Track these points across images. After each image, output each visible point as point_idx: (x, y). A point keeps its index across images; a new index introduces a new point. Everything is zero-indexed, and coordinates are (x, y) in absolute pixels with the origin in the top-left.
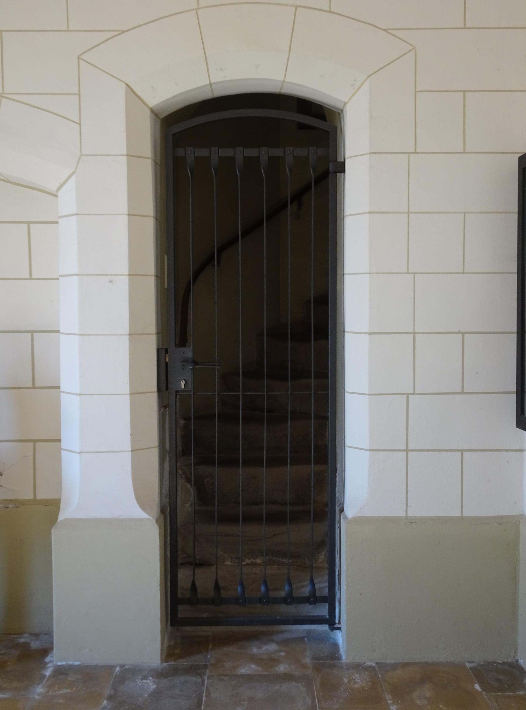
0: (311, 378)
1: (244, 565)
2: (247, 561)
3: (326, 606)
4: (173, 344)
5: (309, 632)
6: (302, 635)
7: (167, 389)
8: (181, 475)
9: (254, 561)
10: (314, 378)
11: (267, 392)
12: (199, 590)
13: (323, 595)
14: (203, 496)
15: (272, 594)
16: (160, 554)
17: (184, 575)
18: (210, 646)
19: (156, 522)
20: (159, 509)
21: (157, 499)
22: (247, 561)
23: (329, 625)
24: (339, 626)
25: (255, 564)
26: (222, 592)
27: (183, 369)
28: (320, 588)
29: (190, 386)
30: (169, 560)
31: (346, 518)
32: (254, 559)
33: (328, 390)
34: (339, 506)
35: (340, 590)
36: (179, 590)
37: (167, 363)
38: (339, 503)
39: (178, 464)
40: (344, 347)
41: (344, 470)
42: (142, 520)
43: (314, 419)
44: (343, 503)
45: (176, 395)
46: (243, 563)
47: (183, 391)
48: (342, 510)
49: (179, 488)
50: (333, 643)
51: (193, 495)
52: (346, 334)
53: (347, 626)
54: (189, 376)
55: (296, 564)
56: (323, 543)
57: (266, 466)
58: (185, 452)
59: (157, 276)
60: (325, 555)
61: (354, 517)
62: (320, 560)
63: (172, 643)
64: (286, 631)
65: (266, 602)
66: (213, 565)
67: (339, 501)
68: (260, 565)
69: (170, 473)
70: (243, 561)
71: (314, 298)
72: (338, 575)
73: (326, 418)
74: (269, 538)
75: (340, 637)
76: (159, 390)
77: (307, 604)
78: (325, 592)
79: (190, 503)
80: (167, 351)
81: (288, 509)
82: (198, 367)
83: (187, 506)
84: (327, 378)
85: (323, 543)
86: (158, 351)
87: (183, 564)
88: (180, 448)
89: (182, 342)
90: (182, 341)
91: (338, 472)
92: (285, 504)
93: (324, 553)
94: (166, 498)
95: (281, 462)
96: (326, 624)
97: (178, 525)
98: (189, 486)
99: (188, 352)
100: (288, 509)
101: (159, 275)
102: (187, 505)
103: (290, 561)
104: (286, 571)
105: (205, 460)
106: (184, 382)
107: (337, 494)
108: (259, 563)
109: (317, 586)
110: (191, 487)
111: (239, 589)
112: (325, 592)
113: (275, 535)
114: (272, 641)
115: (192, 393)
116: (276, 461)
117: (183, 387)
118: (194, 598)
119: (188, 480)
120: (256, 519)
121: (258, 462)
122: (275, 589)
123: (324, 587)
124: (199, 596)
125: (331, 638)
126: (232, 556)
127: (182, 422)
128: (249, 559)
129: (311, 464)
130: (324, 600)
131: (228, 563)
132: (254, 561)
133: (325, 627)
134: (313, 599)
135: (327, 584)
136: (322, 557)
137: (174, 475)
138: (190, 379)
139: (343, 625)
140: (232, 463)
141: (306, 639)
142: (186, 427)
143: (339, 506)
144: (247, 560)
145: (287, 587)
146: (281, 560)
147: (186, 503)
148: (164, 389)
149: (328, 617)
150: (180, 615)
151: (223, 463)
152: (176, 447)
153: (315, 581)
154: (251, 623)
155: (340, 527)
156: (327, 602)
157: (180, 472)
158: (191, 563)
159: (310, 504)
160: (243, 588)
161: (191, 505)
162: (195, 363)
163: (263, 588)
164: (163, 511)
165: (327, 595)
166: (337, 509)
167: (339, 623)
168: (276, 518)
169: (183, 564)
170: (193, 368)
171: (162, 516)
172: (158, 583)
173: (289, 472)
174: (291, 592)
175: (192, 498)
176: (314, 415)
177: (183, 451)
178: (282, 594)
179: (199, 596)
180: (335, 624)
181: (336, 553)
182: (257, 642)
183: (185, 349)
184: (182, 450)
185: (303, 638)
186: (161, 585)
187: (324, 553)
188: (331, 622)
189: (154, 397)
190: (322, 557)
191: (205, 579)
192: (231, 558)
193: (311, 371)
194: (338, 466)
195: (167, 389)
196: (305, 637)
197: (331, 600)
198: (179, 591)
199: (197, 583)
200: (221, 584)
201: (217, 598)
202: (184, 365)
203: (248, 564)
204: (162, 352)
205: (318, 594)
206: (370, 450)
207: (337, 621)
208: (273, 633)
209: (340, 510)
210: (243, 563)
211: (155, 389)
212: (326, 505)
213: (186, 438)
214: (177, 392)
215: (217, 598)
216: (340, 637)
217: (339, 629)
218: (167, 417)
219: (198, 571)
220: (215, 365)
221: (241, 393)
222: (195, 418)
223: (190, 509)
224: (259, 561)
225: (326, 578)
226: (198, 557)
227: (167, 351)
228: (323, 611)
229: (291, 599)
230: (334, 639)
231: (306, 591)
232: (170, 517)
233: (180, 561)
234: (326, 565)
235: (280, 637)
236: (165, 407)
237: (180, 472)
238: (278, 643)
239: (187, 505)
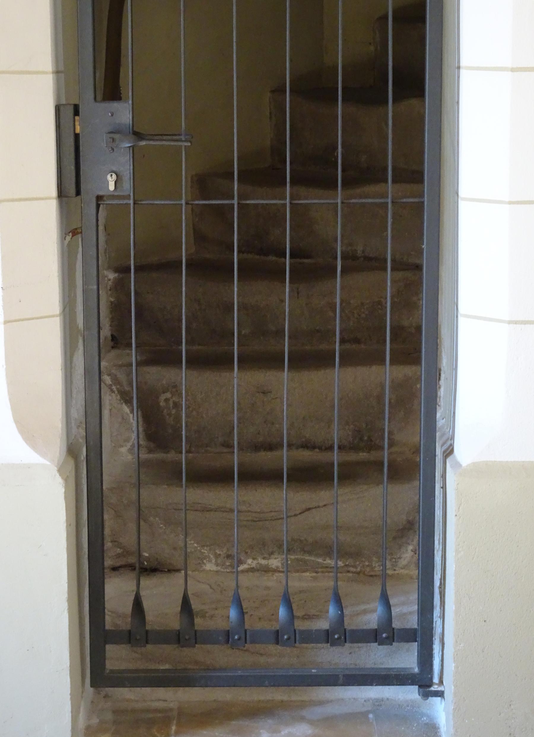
0: (386, 181)
1: (242, 571)
2: (250, 563)
3: (414, 646)
4: (90, 95)
5: (378, 703)
6: (364, 709)
7: (78, 193)
8: (110, 387)
9: (263, 562)
10: (394, 181)
11: (292, 198)
12: (150, 617)
13: (408, 626)
14: (157, 431)
15: (300, 625)
16: (60, 296)
17: (118, 591)
18: (174, 728)
19: (59, 471)
20: (65, 449)
21: (60, 425)
22: (250, 563)
23: (420, 687)
24: (440, 689)
25: (267, 570)
26: (198, 621)
27: (113, 149)
28: (403, 615)
29: (127, 186)
30: (86, 556)
31: (458, 465)
32: (264, 558)
33: (423, 197)
34: (442, 446)
35: (443, 617)
36: (107, 618)
37: (77, 137)
38: (444, 438)
39: (103, 364)
40: (458, 103)
41: (455, 368)
42: (29, 466)
43: (392, 269)
44: (453, 438)
45: (98, 206)
46: (241, 568)
47: (112, 197)
48: (449, 452)
49: (106, 413)
50: (426, 724)
51: (135, 428)
52: (463, 72)
53: (456, 686)
54: (124, 162)
55: (352, 569)
56: (408, 527)
57: (289, 367)
58: (118, 341)
59: (57, 72)
60: (414, 551)
61: (474, 464)
62: (403, 562)
63: (95, 721)
64: (328, 702)
65: (289, 639)
66: (178, 570)
67: (443, 435)
68: (276, 571)
69: (87, 372)
70: (240, 562)
71: (394, 12)
72: (440, 588)
73: (418, 268)
74: (295, 515)
75: (441, 711)
76: (61, 194)
77: (376, 644)
78: (413, 622)
79: (129, 445)
80: (76, 112)
81: (336, 457)
82: (143, 143)
83: (123, 449)
84: (422, 181)
85: (408, 527)
86: (58, 109)
87: (114, 569)
88: (106, 332)
89: (112, 92)
90: (111, 90)
91: (443, 376)
92: (330, 448)
93: (410, 547)
94: (78, 427)
95: (323, 360)
96: (412, 684)
97: (104, 488)
98: (126, 409)
99: (123, 113)
100: (336, 457)
101: (62, 68)
102: (124, 450)
103: (340, 564)
104: (332, 583)
105: (161, 356)
106: (114, 176)
107: (440, 423)
108: (273, 566)
109: (395, 611)
110: (132, 411)
111: (233, 613)
112: (413, 622)
113: (309, 509)
114: (302, 719)
115: (131, 202)
116: (310, 358)
117: (112, 187)
118: (138, 631)
119: (126, 398)
120: (270, 477)
121: (273, 361)
122: (307, 617)
123: (411, 613)
124: (148, 627)
125: (423, 715)
126: (218, 552)
127: (112, 276)
128: (254, 559)
129: (385, 364)
130: (409, 636)
131: (210, 566)
132: (263, 562)
133: (410, 693)
134: (386, 634)
135: (416, 607)
136: (408, 554)
137: (94, 377)
138: (127, 170)
139: (448, 687)
140: (221, 362)
141: (371, 716)
142: (120, 286)
143: (442, 446)
144: (250, 561)
145: (332, 610)
146: (320, 560)
147: (122, 446)
148: (72, 190)
149: (416, 670)
150: (110, 665)
151: (197, 362)
152: (99, 328)
153: (392, 602)
154: (258, 681)
155: (444, 487)
156: (416, 641)
157: (107, 379)
158: (131, 567)
159: (382, 448)
160: (242, 613)
161: (130, 451)
162: (138, 135)
163: (282, 612)
164: (71, 451)
165: (416, 626)
166: (439, 451)
167: (441, 682)
168: (309, 476)
169: (114, 569)
170: (133, 147)
171: (72, 462)
172: (66, 596)
173: (339, 381)
174: (341, 619)
175: (134, 436)
176: (393, 260)
177: (113, 338)
178: (324, 625)
179: (148, 627)
180: (431, 685)
181: (436, 542)
182: (270, 721)
183: (115, 105)
184: (112, 336)
185: (365, 714)
186: (69, 600)
187: (410, 547)
188: (423, 680)
189: (51, 208)
190: (408, 554)
191: (161, 599)
192: (217, 556)
193: (386, 169)
194: (444, 363)
195: (78, 193)
196: (368, 712)
197: (423, 636)
198: (108, 619)
199: (146, 604)
200: (195, 605)
201: (187, 635)
202: (114, 140)
203: (252, 570)
204: (67, 113)
205: (396, 624)
206: (510, 322)
207: (436, 680)
208: (303, 705)
209: (444, 452)
210: (241, 568)
211: (53, 191)
212: (417, 451)
213: (119, 310)
214: (99, 198)
215: (187, 635)
216: (441, 711)
217: (440, 694)
218: (80, 256)
219: (145, 582)
220: (180, 140)
221: (235, 202)
222: (139, 269)
223: (130, 457)
224: (275, 562)
225: (414, 597)
226: (146, 555)
227: (76, 112)
228: (407, 658)
229: (339, 635)
230: (428, 716)
231: (372, 619)
232: (86, 459)
233: (108, 563)
234: (414, 572)
235: (319, 711)
236: (74, 232)
237: (107, 379)
238: (311, 722)
239: (124, 450)
